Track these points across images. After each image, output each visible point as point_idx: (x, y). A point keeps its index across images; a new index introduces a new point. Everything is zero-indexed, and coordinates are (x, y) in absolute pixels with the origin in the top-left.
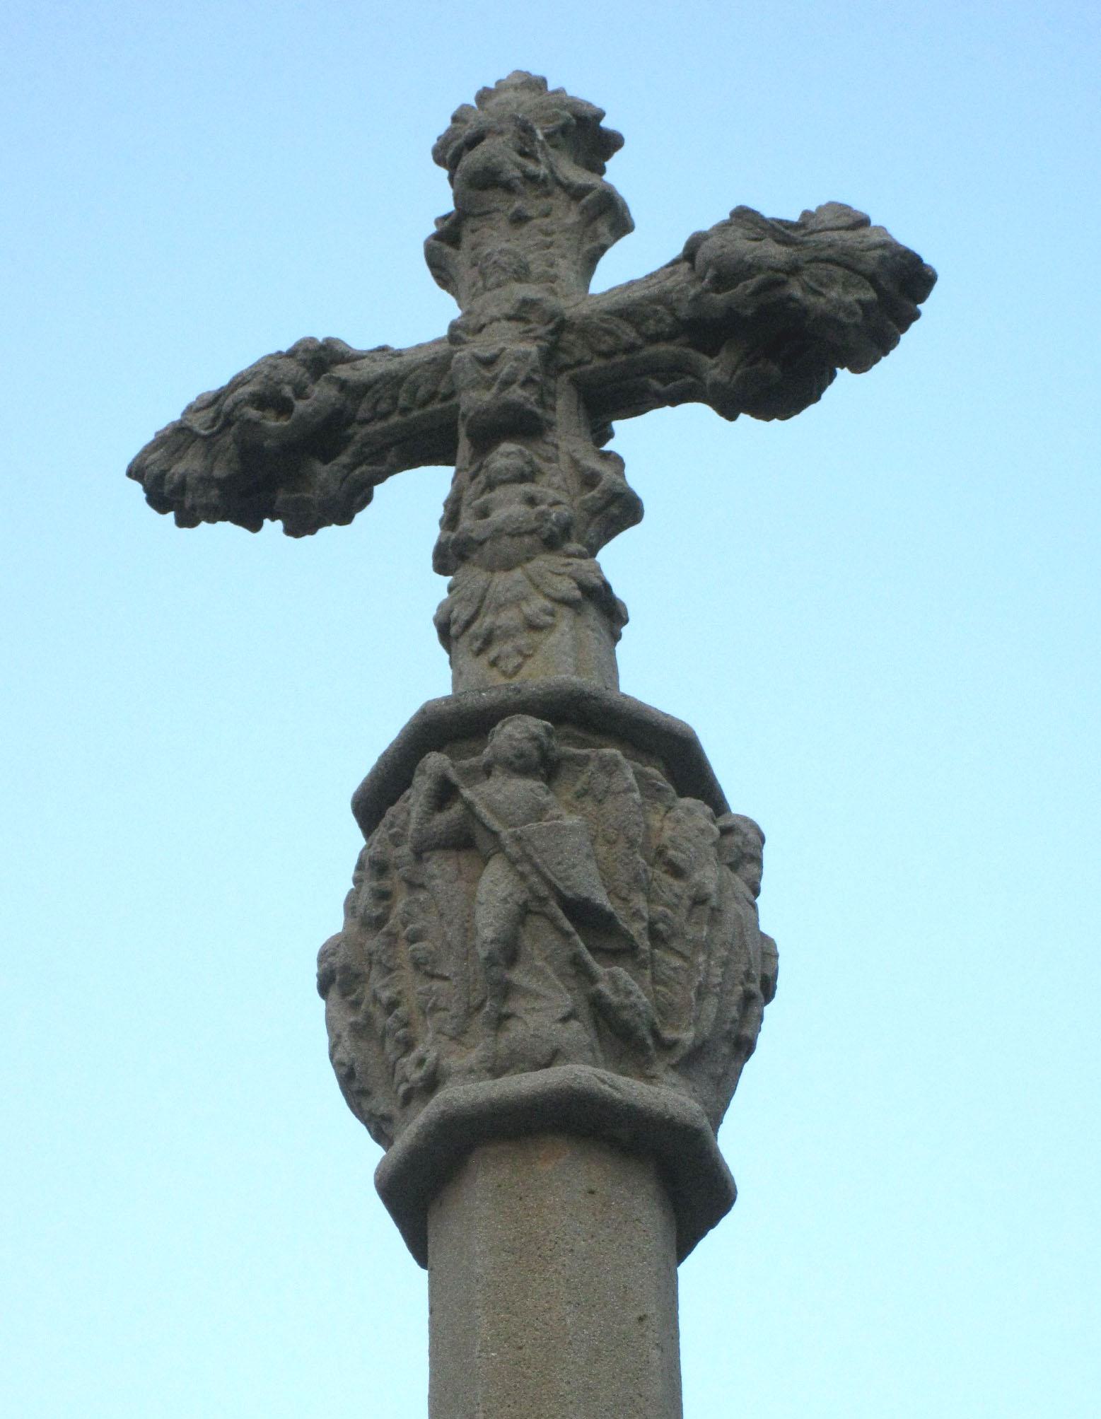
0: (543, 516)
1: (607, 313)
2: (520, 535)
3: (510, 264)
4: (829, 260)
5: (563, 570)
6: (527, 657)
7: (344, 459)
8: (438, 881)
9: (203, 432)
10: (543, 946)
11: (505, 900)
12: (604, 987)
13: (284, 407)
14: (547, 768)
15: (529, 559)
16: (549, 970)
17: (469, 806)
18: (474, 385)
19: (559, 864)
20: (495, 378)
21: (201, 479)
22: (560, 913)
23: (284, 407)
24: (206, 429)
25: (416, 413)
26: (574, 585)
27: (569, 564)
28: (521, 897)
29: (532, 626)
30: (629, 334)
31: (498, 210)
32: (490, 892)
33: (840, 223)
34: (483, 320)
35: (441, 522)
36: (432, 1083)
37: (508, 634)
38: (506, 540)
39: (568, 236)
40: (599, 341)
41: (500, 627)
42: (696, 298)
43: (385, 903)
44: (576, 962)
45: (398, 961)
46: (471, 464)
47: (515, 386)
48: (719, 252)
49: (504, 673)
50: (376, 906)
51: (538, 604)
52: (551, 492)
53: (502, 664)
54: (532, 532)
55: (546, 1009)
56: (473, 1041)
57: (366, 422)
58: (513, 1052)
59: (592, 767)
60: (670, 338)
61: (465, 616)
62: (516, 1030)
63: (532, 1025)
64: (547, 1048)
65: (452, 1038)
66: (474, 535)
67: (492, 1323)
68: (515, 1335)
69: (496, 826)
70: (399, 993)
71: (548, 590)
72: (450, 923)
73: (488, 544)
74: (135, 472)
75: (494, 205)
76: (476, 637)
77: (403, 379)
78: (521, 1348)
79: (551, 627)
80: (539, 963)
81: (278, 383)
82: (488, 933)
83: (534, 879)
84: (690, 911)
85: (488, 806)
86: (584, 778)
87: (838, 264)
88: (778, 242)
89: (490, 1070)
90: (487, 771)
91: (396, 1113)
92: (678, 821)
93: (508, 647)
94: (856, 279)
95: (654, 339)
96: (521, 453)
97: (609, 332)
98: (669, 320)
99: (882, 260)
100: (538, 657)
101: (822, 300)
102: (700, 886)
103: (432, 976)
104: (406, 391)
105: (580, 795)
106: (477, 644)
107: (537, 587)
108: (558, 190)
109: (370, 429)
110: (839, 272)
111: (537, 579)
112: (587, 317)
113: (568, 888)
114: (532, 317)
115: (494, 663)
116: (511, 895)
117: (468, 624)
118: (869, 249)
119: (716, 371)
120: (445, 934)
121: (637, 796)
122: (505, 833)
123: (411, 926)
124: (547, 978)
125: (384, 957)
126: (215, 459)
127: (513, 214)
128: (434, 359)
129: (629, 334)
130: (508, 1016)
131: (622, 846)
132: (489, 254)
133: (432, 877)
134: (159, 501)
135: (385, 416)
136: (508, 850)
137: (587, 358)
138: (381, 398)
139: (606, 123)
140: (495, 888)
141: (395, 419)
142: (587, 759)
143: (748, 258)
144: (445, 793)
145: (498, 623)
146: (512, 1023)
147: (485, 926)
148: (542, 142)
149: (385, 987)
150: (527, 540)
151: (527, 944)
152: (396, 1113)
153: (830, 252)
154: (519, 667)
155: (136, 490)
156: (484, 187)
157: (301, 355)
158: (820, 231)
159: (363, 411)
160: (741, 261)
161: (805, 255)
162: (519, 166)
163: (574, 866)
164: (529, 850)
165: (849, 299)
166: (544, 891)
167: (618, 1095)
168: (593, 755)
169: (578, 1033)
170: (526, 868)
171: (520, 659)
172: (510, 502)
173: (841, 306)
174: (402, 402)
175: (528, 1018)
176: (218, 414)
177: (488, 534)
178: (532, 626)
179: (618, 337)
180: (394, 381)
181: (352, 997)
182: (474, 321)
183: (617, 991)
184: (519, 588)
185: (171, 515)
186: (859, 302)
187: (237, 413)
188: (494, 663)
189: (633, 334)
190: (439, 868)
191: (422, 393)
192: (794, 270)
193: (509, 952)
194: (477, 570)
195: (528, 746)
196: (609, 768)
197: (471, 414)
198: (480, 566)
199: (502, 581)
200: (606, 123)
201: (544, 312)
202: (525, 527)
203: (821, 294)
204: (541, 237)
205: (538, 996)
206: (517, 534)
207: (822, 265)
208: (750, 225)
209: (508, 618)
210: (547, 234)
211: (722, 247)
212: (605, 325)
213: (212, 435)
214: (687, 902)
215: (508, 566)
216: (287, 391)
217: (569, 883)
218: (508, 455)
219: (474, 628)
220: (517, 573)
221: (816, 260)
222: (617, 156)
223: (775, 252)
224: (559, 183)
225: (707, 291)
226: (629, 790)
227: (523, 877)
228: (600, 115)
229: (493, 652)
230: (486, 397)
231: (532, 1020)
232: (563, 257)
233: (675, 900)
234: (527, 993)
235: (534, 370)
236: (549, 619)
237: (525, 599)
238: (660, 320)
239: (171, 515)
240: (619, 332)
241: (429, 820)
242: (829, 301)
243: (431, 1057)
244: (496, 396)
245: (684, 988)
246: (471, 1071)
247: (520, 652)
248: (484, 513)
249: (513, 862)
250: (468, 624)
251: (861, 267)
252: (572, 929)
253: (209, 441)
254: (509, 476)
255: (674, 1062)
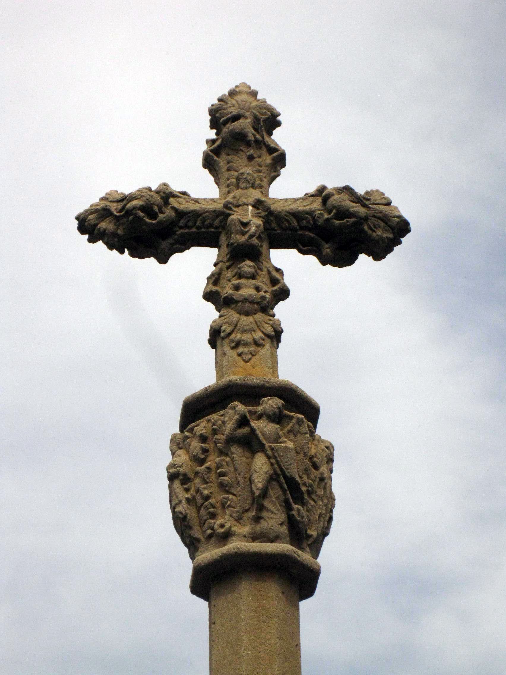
0: (263, 298)
1: (288, 212)
2: (254, 303)
3: (251, 180)
4: (379, 218)
5: (269, 322)
6: (253, 356)
7: (171, 241)
8: (235, 456)
9: (118, 214)
10: (275, 493)
11: (266, 473)
12: (295, 513)
13: (153, 215)
14: (277, 418)
15: (255, 314)
16: (277, 503)
17: (253, 430)
18: (237, 232)
19: (286, 462)
20: (247, 232)
21: (112, 233)
22: (284, 481)
23: (153, 215)
24: (117, 212)
25: (203, 230)
26: (272, 330)
27: (271, 320)
28: (271, 472)
29: (256, 344)
30: (295, 223)
31: (242, 151)
32: (261, 468)
33: (381, 202)
34: (240, 203)
35: (208, 279)
36: (226, 537)
37: (246, 344)
38: (247, 304)
39: (267, 168)
40: (283, 223)
41: (243, 340)
42: (327, 220)
43: (206, 454)
44: (286, 502)
45: (211, 480)
46: (227, 261)
47: (255, 238)
48: (339, 204)
49: (244, 360)
50: (203, 454)
51: (258, 335)
52: (264, 286)
53: (243, 356)
54: (258, 303)
55: (274, 519)
56: (244, 523)
57: (181, 228)
58: (261, 533)
59: (294, 421)
60: (310, 230)
61: (228, 330)
62: (264, 525)
63: (270, 524)
64: (274, 534)
65: (235, 520)
66: (234, 297)
67: (249, 640)
68: (257, 646)
69: (264, 442)
70: (211, 493)
71: (263, 330)
72: (239, 474)
73: (240, 303)
74: (77, 218)
75: (241, 148)
76: (232, 341)
77: (201, 215)
78: (259, 652)
79: (262, 346)
80: (274, 500)
81: (153, 204)
82: (260, 485)
83: (276, 466)
84: (318, 484)
85: (261, 432)
86: (291, 425)
87: (382, 220)
88: (362, 205)
89: (252, 538)
90: (260, 417)
91: (203, 540)
92: (316, 445)
93: (246, 350)
94: (388, 228)
95: (302, 228)
96: (254, 267)
97: (287, 221)
98: (312, 222)
99: (398, 223)
100: (257, 357)
101: (374, 233)
102: (322, 474)
103: (228, 492)
104: (201, 220)
105: (289, 432)
106: (233, 345)
107: (258, 327)
108: (263, 147)
109: (183, 231)
110: (382, 224)
111: (259, 323)
112: (280, 212)
113: (288, 472)
114: (260, 207)
115: (240, 355)
116: (268, 471)
117: (229, 334)
118: (394, 217)
119: (328, 250)
120: (236, 478)
121: (308, 436)
122: (267, 445)
123: (220, 470)
124: (277, 506)
125: (205, 477)
126: (119, 226)
127: (249, 156)
128: (215, 211)
129: (295, 223)
130: (262, 518)
131: (301, 456)
132: (242, 173)
133: (233, 453)
134: (82, 229)
135: (189, 228)
136: (267, 452)
137: (276, 228)
138: (190, 220)
139: (279, 118)
140: (261, 465)
141: (194, 230)
142: (291, 418)
143: (351, 210)
144: (243, 422)
145: (243, 338)
146: (262, 521)
147: (259, 482)
148: (262, 126)
149: (204, 488)
150: (256, 306)
151: (271, 492)
152: (203, 540)
153: (380, 215)
154: (250, 359)
155: (76, 222)
156: (237, 139)
157: (162, 194)
158: (376, 204)
159: (182, 222)
160: (348, 210)
161: (370, 213)
162: (254, 135)
163: (291, 464)
164: (276, 454)
165: (384, 236)
166: (279, 472)
167: (299, 559)
168: (295, 416)
169: (284, 530)
170: (273, 461)
171: (250, 356)
172: (250, 287)
173: (381, 238)
174: (198, 224)
175: (269, 521)
176: (124, 207)
177: (241, 299)
178: (256, 344)
179: (290, 224)
180: (196, 214)
181: (186, 486)
182: (236, 202)
183: (299, 515)
184: (252, 326)
185: (87, 236)
186: (387, 237)
187: (134, 212)
188: (240, 355)
189: (296, 224)
190: (236, 450)
191: (207, 222)
192: (366, 219)
193: (264, 493)
194: (233, 312)
195: (277, 410)
196: (299, 422)
197: (236, 244)
198: (235, 310)
199: (246, 321)
200: (279, 118)
201: (265, 206)
202: (256, 301)
203: (374, 231)
204: (257, 167)
205: (273, 513)
206: (252, 302)
207: (376, 220)
208: (351, 195)
209: (246, 337)
210: (260, 166)
211: (340, 202)
212: (286, 218)
213: (120, 216)
214: (318, 479)
215: (247, 314)
216: (156, 209)
217: (289, 471)
218: (250, 266)
219: (232, 337)
220: (251, 319)
221: (374, 216)
222: (278, 129)
223: (362, 211)
224: (264, 143)
225: (331, 218)
226: (306, 433)
227: (272, 464)
228: (279, 115)
229: (240, 350)
230: (242, 239)
231: (271, 522)
232: (265, 177)
233: (314, 478)
234: (268, 510)
235: (262, 233)
236: (262, 342)
237: (254, 331)
238: (308, 222)
239: (87, 236)
240: (291, 222)
241: (235, 431)
242: (377, 235)
243: (227, 526)
244: (247, 240)
245: (314, 514)
246: (245, 536)
247: (251, 353)
248: (237, 288)
249: (269, 458)
250: (229, 334)
251: (391, 223)
252: (287, 489)
253: (117, 219)
254: (249, 276)
255: (309, 542)
